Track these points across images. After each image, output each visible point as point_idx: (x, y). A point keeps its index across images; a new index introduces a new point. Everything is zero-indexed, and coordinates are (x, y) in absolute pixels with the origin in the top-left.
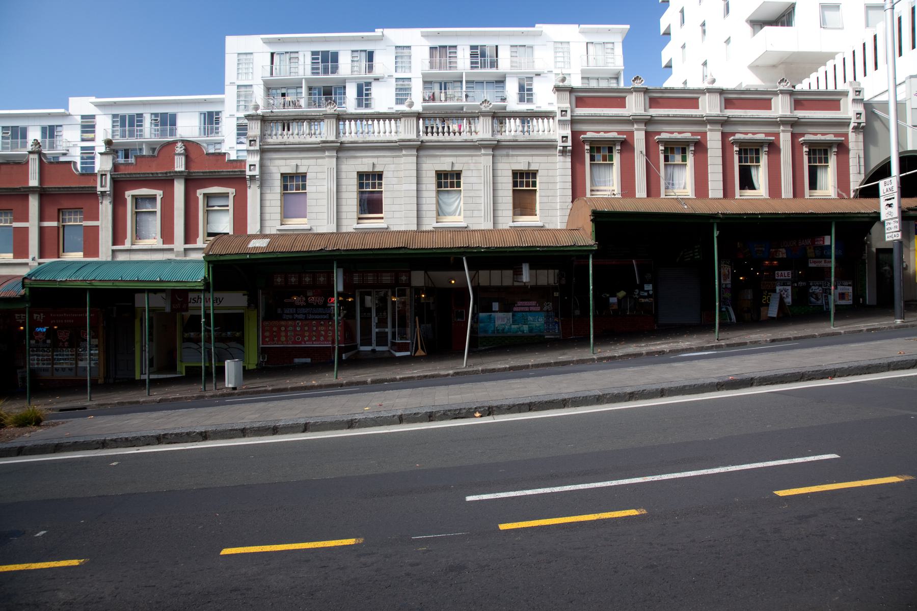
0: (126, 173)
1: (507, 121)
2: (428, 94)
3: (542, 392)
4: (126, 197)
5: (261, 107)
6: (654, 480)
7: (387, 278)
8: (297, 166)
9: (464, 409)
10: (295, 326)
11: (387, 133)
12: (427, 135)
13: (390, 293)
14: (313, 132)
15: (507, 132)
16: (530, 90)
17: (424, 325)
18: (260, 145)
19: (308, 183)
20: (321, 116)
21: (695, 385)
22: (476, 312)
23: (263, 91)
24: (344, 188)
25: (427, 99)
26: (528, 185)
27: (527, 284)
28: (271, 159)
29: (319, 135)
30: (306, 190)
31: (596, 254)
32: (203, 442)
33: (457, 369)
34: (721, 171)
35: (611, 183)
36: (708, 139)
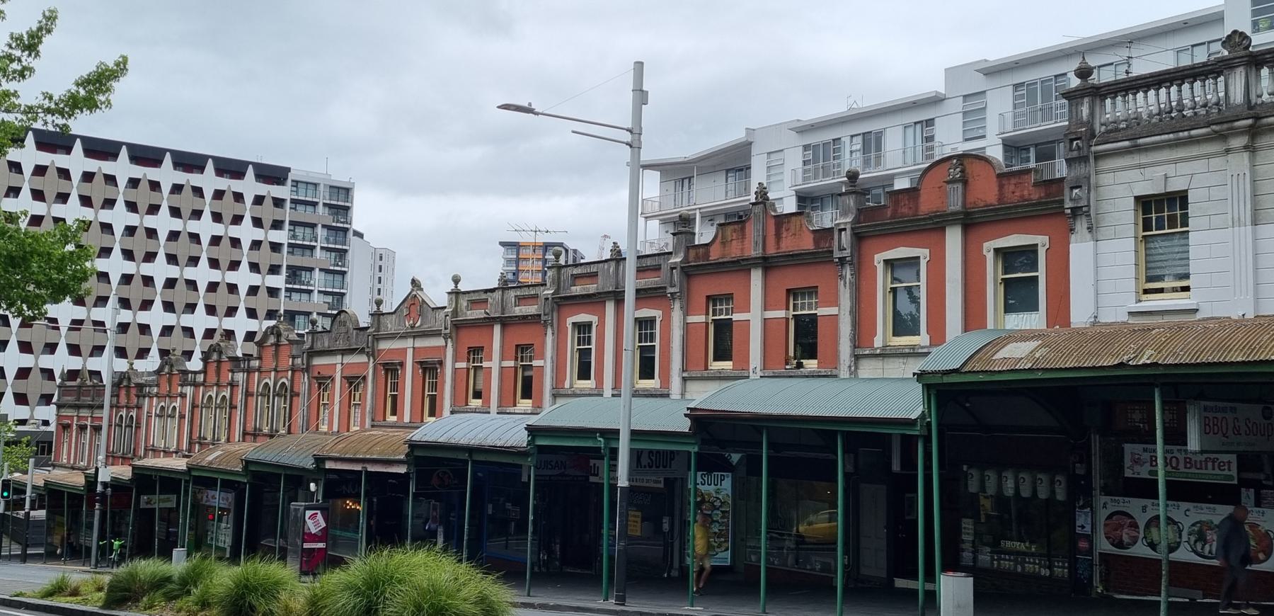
4: (876, 264)
8: (1166, 177)
30: (1187, 226)
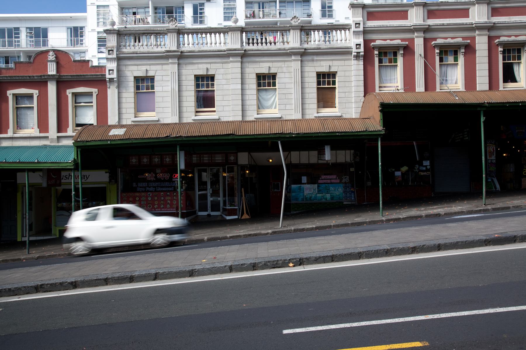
0: (7, 76)
1: (312, 33)
2: (250, 12)
3: (342, 247)
5: (117, 23)
6: (434, 318)
7: (219, 158)
8: (147, 70)
9: (281, 260)
10: (147, 197)
11: (218, 44)
12: (249, 45)
13: (221, 170)
14: (159, 43)
15: (312, 42)
16: (331, 7)
17: (248, 195)
18: (117, 54)
19: (155, 84)
20: (165, 31)
21: (466, 241)
22: (289, 184)
23: (118, 10)
24: (184, 88)
25: (249, 16)
26: (329, 84)
27: (328, 162)
28: (126, 65)
29: (164, 46)
31: (384, 138)
32: (73, 290)
33: (275, 229)
34: (487, 68)
35: (396, 81)
36: (476, 43)
